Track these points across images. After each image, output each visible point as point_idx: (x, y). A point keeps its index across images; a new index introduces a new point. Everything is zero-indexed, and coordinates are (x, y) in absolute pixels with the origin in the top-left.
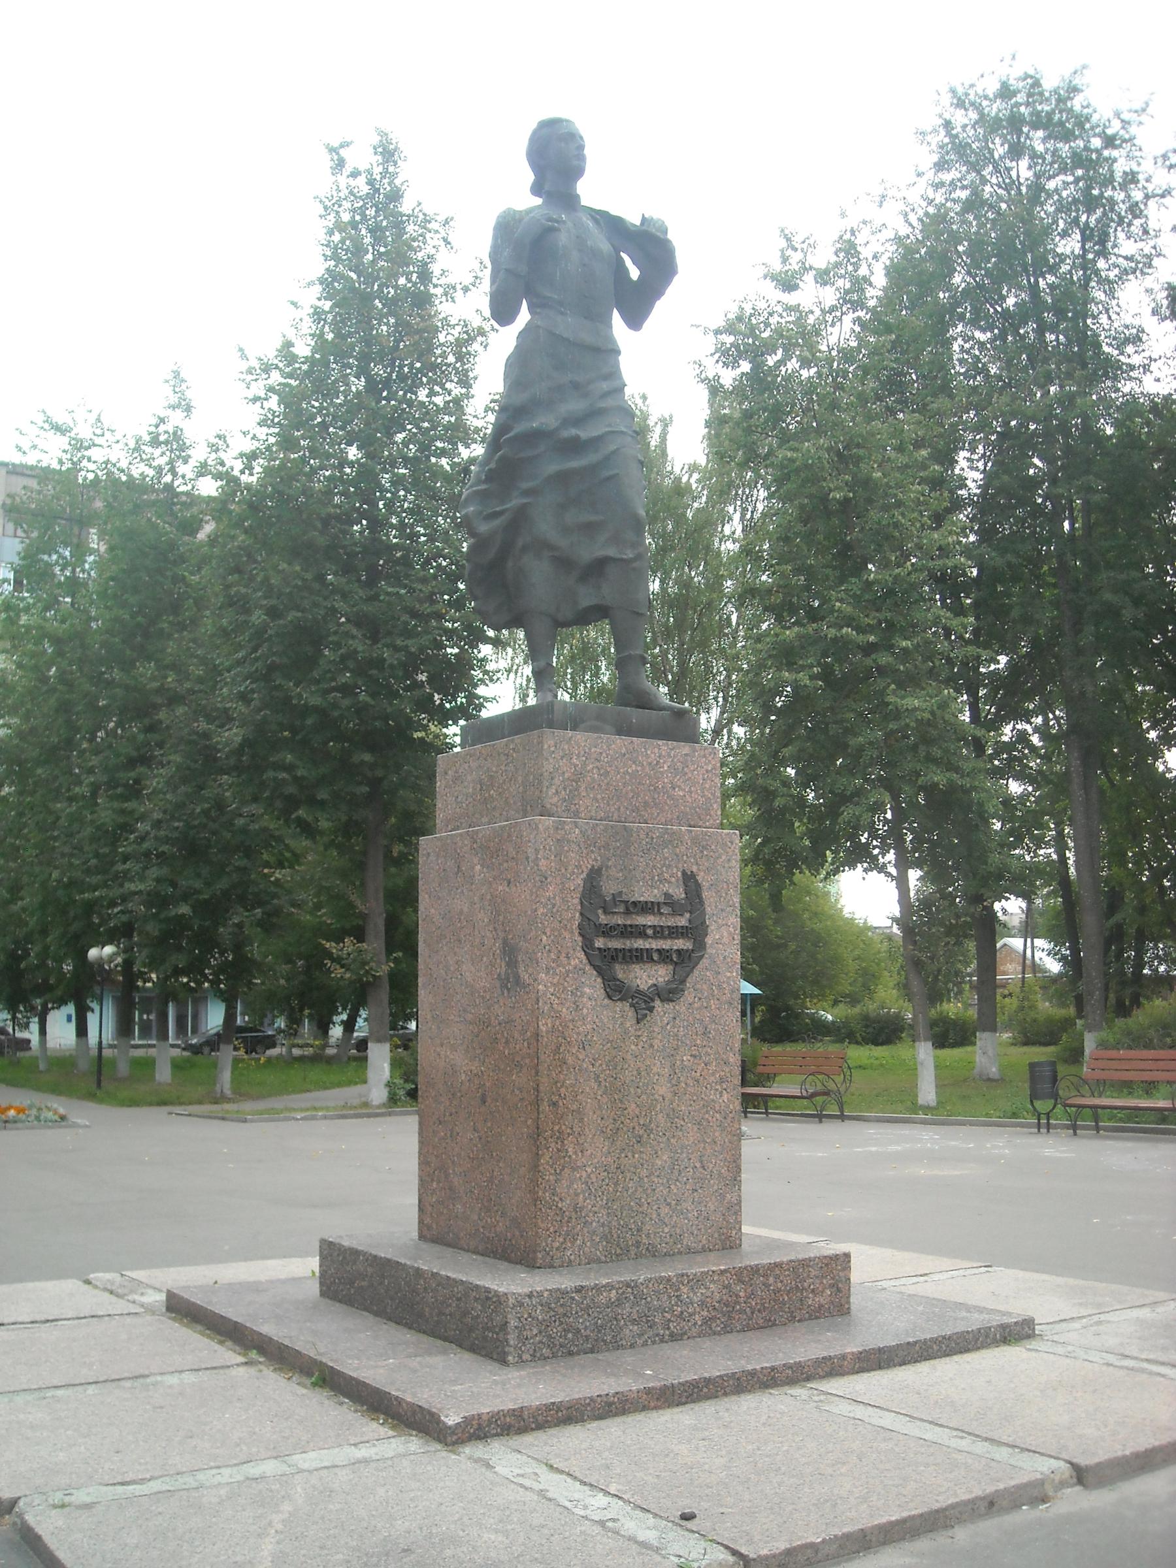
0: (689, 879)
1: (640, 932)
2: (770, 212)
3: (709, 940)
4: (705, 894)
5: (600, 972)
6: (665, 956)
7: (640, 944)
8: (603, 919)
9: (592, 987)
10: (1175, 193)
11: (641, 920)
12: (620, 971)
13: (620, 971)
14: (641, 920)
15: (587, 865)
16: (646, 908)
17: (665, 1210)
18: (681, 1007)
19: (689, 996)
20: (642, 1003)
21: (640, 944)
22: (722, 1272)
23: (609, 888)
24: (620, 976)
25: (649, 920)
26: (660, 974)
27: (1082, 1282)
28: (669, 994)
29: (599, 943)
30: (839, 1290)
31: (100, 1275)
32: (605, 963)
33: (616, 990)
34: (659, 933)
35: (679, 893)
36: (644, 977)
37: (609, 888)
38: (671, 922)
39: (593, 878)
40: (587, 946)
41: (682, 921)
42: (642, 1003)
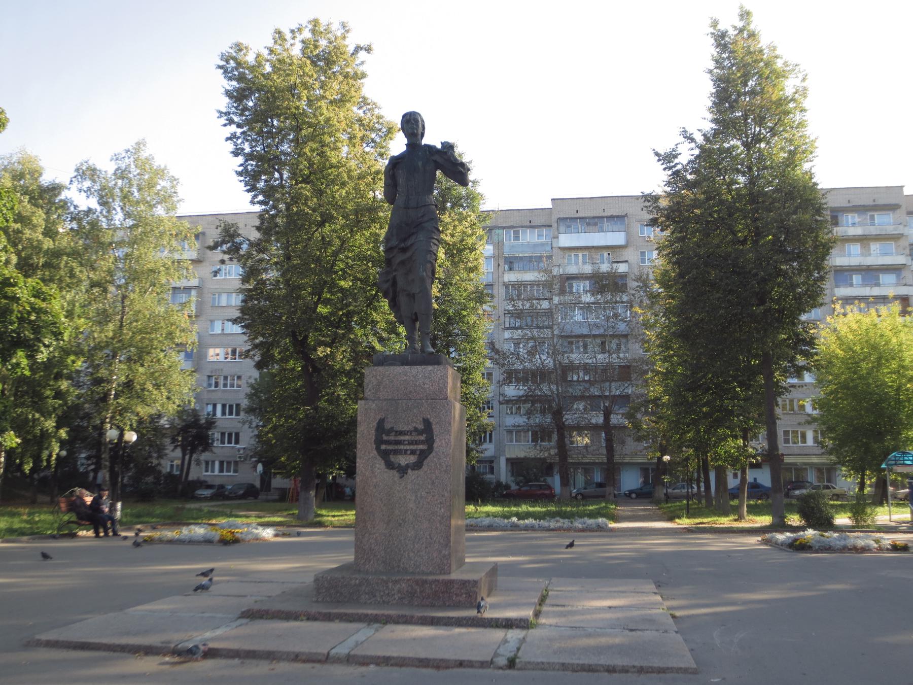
0: (427, 423)
1: (398, 443)
2: (479, 189)
3: (435, 445)
4: (433, 427)
5: (383, 458)
6: (413, 452)
7: (402, 447)
8: (385, 438)
9: (380, 464)
10: (716, 16)
11: (402, 438)
12: (392, 458)
13: (392, 458)
14: (402, 438)
15: (378, 417)
16: (401, 433)
17: (411, 554)
18: (421, 472)
19: (425, 468)
20: (403, 471)
21: (402, 447)
22: (408, 580)
23: (387, 426)
24: (392, 460)
25: (407, 438)
26: (412, 459)
27: (498, 509)
28: (418, 466)
29: (383, 447)
30: (470, 596)
31: (617, 640)
32: (385, 455)
33: (390, 465)
34: (411, 443)
35: (421, 427)
36: (403, 460)
37: (387, 426)
38: (417, 438)
39: (381, 423)
40: (378, 449)
41: (423, 438)
42: (403, 471)
